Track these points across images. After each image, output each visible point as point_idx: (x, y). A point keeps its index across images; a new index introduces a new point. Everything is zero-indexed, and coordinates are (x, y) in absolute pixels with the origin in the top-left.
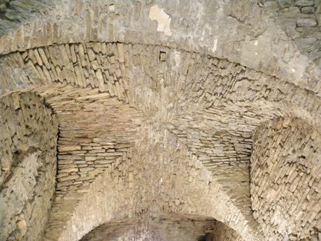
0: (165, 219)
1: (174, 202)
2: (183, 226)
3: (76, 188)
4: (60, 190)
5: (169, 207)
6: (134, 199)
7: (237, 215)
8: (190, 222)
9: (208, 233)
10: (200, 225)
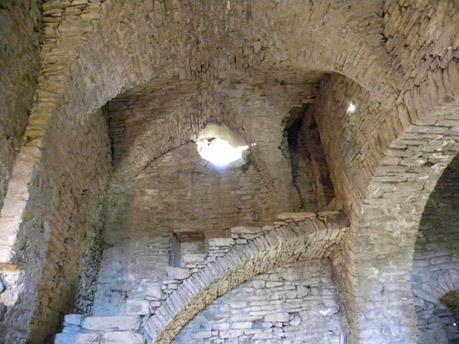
0: (239, 82)
1: (252, 47)
2: (267, 92)
3: (77, 11)
4: (49, 16)
5: (244, 57)
6: (186, 44)
7: (357, 50)
8: (279, 86)
9: (308, 104)
10: (293, 90)
